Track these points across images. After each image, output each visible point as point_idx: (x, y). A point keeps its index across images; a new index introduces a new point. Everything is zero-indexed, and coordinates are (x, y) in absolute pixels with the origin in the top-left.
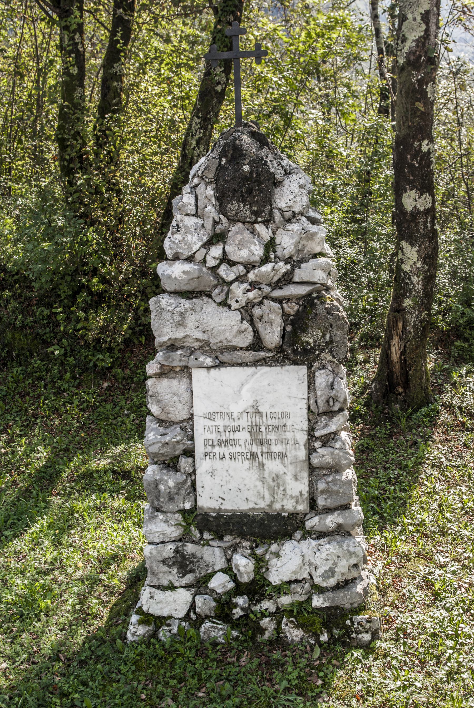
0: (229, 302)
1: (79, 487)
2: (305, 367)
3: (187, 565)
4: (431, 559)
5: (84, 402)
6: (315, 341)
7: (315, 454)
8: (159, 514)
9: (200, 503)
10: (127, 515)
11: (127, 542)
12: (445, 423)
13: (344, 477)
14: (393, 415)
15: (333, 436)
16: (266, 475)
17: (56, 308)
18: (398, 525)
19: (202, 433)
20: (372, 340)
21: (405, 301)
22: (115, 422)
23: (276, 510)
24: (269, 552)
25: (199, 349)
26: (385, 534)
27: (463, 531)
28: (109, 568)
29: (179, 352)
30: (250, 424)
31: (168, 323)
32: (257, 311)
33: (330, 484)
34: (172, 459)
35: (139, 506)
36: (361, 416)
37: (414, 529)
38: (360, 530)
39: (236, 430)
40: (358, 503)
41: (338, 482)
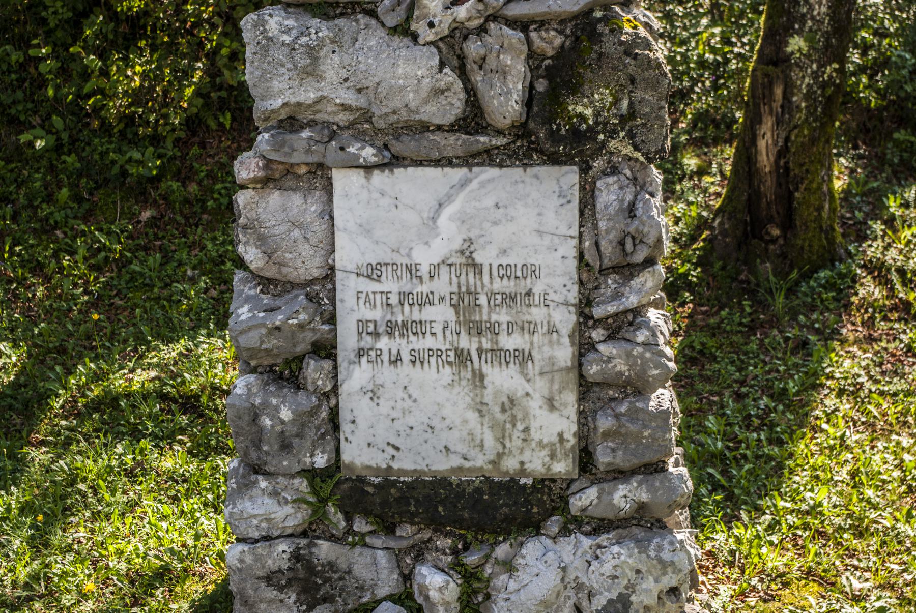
0: (414, 26)
1: (87, 427)
2: (575, 168)
3: (318, 587)
4: (833, 584)
5: (99, 250)
6: (597, 114)
7: (591, 356)
8: (260, 477)
9: (346, 457)
10: (193, 488)
11: (191, 543)
12: (865, 305)
13: (653, 403)
14: (758, 285)
15: (630, 318)
16: (488, 399)
17: (39, 46)
18: (764, 513)
19: (354, 306)
20: (717, 126)
21: (791, 41)
22: (166, 293)
23: (507, 473)
24: (492, 561)
25: (348, 128)
26: (736, 531)
27: (902, 527)
28: (152, 595)
29: (306, 134)
30: (455, 290)
31: (282, 70)
32: (473, 48)
33: (624, 419)
34: (287, 362)
35: (216, 469)
36: (690, 286)
37: (798, 523)
38: (683, 516)
39: (427, 301)
40: (681, 461)
41: (641, 416)
